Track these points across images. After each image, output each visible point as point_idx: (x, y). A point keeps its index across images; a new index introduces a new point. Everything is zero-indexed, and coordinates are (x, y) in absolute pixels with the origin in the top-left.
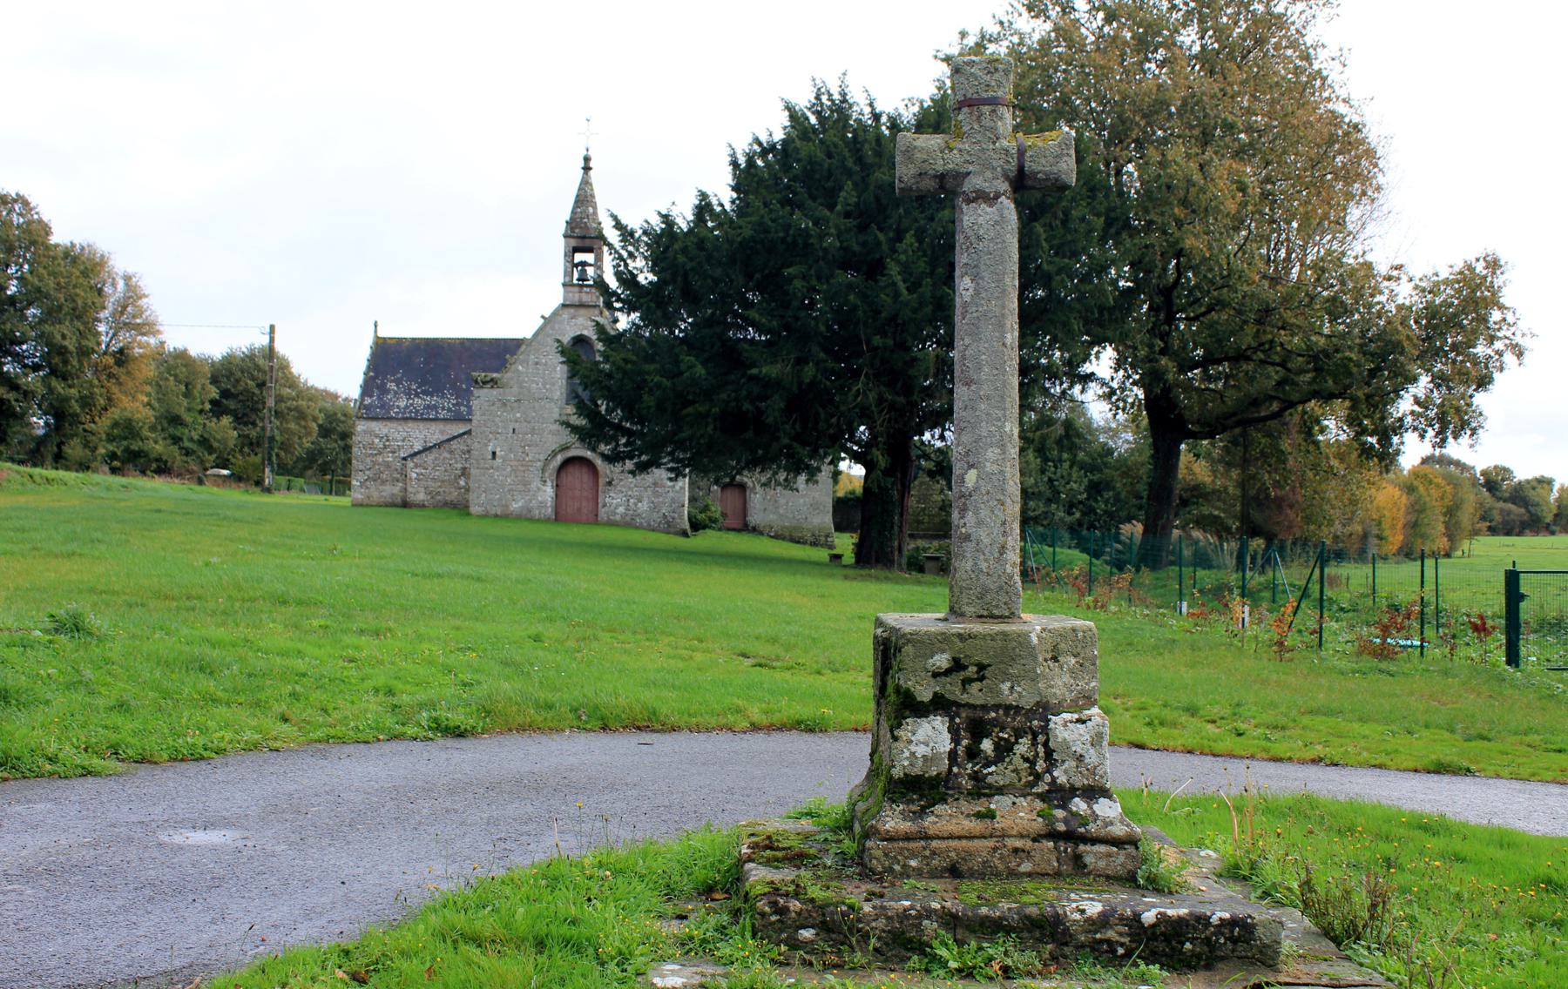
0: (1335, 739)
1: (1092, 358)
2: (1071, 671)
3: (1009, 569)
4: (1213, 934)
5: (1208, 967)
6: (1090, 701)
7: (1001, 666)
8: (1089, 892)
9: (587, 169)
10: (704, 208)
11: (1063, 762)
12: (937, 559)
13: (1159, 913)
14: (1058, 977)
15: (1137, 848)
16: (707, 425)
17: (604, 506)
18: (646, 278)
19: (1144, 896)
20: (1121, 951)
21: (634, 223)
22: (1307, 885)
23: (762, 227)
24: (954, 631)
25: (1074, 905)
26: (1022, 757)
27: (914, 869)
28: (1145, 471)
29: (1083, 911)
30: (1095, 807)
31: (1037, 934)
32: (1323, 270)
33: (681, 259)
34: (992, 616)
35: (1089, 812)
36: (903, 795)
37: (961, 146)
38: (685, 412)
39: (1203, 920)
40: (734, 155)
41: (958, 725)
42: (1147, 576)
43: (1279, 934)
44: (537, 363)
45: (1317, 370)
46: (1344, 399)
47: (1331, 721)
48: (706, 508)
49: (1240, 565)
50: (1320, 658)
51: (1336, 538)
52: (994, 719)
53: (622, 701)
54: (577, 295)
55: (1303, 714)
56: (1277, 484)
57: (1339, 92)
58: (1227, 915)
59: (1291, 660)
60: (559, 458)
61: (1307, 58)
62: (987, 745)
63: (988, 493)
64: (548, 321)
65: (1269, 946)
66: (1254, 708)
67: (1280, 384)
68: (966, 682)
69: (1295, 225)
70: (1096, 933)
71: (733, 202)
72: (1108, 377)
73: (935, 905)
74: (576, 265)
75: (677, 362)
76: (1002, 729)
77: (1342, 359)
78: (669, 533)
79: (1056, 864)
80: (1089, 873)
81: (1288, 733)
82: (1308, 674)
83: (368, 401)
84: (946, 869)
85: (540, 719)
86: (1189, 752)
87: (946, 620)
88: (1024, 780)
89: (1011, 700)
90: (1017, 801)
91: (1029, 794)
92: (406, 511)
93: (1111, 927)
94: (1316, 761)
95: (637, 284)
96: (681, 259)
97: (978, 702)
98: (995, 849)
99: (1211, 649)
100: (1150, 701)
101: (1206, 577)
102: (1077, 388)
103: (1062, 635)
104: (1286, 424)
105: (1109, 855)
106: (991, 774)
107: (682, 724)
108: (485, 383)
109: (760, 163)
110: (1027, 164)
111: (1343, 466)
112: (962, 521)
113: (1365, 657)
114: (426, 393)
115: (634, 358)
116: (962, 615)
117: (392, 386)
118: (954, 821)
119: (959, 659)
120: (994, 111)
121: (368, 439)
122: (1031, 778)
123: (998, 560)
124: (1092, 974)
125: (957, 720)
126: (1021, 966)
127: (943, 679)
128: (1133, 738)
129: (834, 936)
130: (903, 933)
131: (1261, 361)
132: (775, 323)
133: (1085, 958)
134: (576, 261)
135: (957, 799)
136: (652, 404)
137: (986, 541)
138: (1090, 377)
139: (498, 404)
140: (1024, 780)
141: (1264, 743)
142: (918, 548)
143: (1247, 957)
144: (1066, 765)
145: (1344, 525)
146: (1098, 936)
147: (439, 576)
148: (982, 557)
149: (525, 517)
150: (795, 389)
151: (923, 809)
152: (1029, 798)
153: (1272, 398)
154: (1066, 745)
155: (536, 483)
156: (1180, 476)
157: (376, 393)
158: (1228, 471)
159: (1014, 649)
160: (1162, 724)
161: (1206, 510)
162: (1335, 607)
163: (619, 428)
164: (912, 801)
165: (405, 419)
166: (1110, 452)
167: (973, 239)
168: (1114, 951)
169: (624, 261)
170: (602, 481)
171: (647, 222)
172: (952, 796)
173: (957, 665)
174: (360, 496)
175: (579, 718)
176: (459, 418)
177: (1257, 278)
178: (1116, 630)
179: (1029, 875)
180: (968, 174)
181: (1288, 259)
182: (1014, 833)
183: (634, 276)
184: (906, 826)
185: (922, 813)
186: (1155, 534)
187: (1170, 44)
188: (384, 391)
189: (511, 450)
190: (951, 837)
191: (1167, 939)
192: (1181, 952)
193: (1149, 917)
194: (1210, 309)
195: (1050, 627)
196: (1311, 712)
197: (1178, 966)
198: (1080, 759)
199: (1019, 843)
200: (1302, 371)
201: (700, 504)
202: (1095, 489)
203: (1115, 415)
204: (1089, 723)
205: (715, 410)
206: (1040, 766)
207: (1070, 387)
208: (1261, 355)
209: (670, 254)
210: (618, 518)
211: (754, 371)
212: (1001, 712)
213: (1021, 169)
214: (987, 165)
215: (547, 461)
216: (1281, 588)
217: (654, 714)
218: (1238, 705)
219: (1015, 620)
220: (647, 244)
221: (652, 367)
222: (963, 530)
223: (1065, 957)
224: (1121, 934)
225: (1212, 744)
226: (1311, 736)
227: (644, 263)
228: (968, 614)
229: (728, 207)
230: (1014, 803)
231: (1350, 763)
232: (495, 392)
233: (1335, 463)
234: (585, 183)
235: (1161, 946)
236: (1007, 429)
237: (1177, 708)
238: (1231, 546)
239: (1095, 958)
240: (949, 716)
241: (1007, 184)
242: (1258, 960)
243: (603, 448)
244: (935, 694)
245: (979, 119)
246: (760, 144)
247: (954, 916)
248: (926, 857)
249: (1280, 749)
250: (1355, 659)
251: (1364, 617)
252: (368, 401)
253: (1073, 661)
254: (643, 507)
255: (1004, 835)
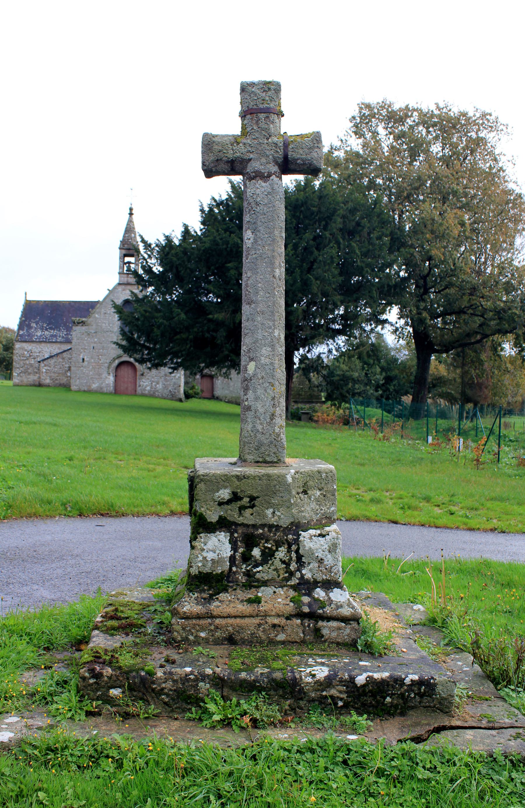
0: (504, 516)
1: (387, 312)
2: (317, 500)
3: (277, 430)
4: (406, 691)
5: (403, 714)
6: (330, 520)
7: (266, 498)
8: (322, 656)
9: (131, 214)
10: (186, 232)
11: (309, 563)
12: (307, 414)
13: (368, 677)
14: (293, 725)
15: (359, 624)
16: (187, 344)
17: (140, 386)
18: (157, 269)
19: (361, 660)
20: (340, 704)
21: (152, 240)
22: (476, 643)
23: (215, 242)
24: (234, 473)
25: (308, 670)
26: (281, 560)
27: (203, 639)
28: (414, 370)
29: (314, 676)
30: (331, 595)
31: (281, 692)
32: (503, 268)
33: (175, 259)
34: (265, 462)
35: (326, 598)
36: (197, 587)
37: (245, 141)
38: (175, 338)
39: (399, 681)
40: (202, 206)
41: (236, 538)
42: (412, 423)
43: (453, 691)
44: (105, 313)
45: (500, 318)
46: (513, 333)
47: (502, 505)
48: (193, 388)
49: (461, 418)
50: (498, 468)
51: (509, 403)
52: (261, 534)
53: (93, 499)
54: (126, 279)
55: (488, 500)
56: (478, 376)
57: (511, 178)
58: (416, 677)
59: (483, 469)
60: (117, 362)
61: (496, 160)
62: (256, 552)
63: (263, 378)
64: (111, 292)
65: (446, 699)
66: (461, 498)
67: (481, 325)
68: (242, 508)
69: (489, 246)
70: (322, 691)
71: (201, 230)
72: (394, 322)
73: (209, 671)
74: (126, 263)
75: (172, 312)
76: (267, 541)
77: (512, 313)
78: (172, 400)
79: (302, 635)
80: (325, 641)
81: (479, 513)
82: (491, 477)
83: (21, 332)
84: (225, 639)
85: (41, 510)
86: (422, 525)
87: (235, 464)
88: (281, 576)
89: (273, 521)
90: (277, 590)
91: (285, 586)
92: (39, 388)
93: (334, 687)
94: (493, 530)
95: (152, 272)
96: (175, 259)
97: (250, 523)
98: (259, 625)
99: (441, 463)
100: (404, 493)
101: (442, 423)
102: (380, 327)
103: (310, 475)
104: (484, 346)
105: (339, 629)
106: (259, 572)
107: (129, 512)
108: (78, 323)
109: (216, 211)
110: (290, 154)
111: (513, 367)
112: (246, 397)
113: (521, 467)
114: (51, 328)
115: (150, 310)
116: (245, 461)
117: (34, 325)
118: (232, 605)
119: (237, 493)
120: (267, 117)
121: (21, 352)
122: (287, 575)
123: (269, 424)
124: (318, 723)
125: (236, 535)
126: (265, 719)
127: (226, 507)
128: (392, 518)
129: (135, 693)
130: (184, 692)
131: (471, 314)
132: (221, 292)
133: (315, 709)
134: (126, 261)
135: (235, 589)
136: (159, 333)
137: (261, 410)
138: (386, 321)
139: (86, 334)
140: (281, 576)
141: (465, 520)
142: (298, 408)
143: (430, 707)
144: (311, 566)
145: (513, 397)
146: (324, 693)
147: (35, 423)
148: (258, 422)
149: (99, 392)
150: (232, 326)
151: (211, 596)
152: (285, 588)
153: (477, 333)
154: (311, 552)
155: (105, 375)
156: (431, 372)
157: (25, 328)
158: (455, 370)
159: (275, 486)
160: (409, 508)
161: (444, 389)
162: (507, 439)
163: (143, 346)
164: (204, 591)
165: (41, 342)
166: (396, 360)
167: (253, 205)
168: (336, 704)
169: (146, 260)
170: (138, 373)
171: (158, 240)
172: (232, 587)
173: (235, 497)
174: (17, 381)
175: (66, 509)
176: (69, 342)
177: (469, 271)
178: (392, 452)
179: (283, 643)
180: (250, 160)
181: (485, 263)
182: (273, 613)
183: (151, 268)
184: (197, 609)
185: (210, 599)
186: (417, 401)
187: (427, 152)
188: (29, 327)
189: (92, 358)
190: (229, 616)
191: (374, 695)
192: (383, 704)
193: (361, 680)
194: (446, 287)
195: (302, 470)
196: (492, 499)
197: (381, 714)
198: (321, 561)
199: (276, 621)
200: (491, 319)
201: (190, 385)
202: (389, 379)
203: (398, 341)
204: (327, 537)
205: (191, 337)
206: (293, 566)
207: (376, 327)
208: (471, 311)
209: (170, 256)
210: (147, 392)
211: (210, 316)
212: (266, 529)
213: (286, 157)
214: (263, 154)
215: (110, 363)
216: (480, 429)
217: (112, 506)
218: (453, 495)
219: (281, 464)
220: (158, 251)
221: (159, 315)
222: (246, 403)
223: (301, 708)
224: (340, 692)
225: (435, 520)
226: (491, 514)
227: (156, 261)
228: (249, 461)
229: (199, 233)
230: (275, 592)
231: (512, 531)
232: (84, 328)
233: (509, 365)
234: (130, 221)
235: (369, 700)
236: (276, 334)
237: (419, 498)
238: (456, 408)
239: (323, 709)
240: (229, 532)
241: (277, 167)
242: (437, 708)
243: (138, 356)
244: (220, 517)
245: (257, 123)
246: (215, 201)
247: (222, 679)
248: (211, 630)
249: (473, 523)
250: (516, 468)
251: (522, 444)
252: (21, 332)
253: (319, 493)
254: (160, 386)
255: (266, 615)
